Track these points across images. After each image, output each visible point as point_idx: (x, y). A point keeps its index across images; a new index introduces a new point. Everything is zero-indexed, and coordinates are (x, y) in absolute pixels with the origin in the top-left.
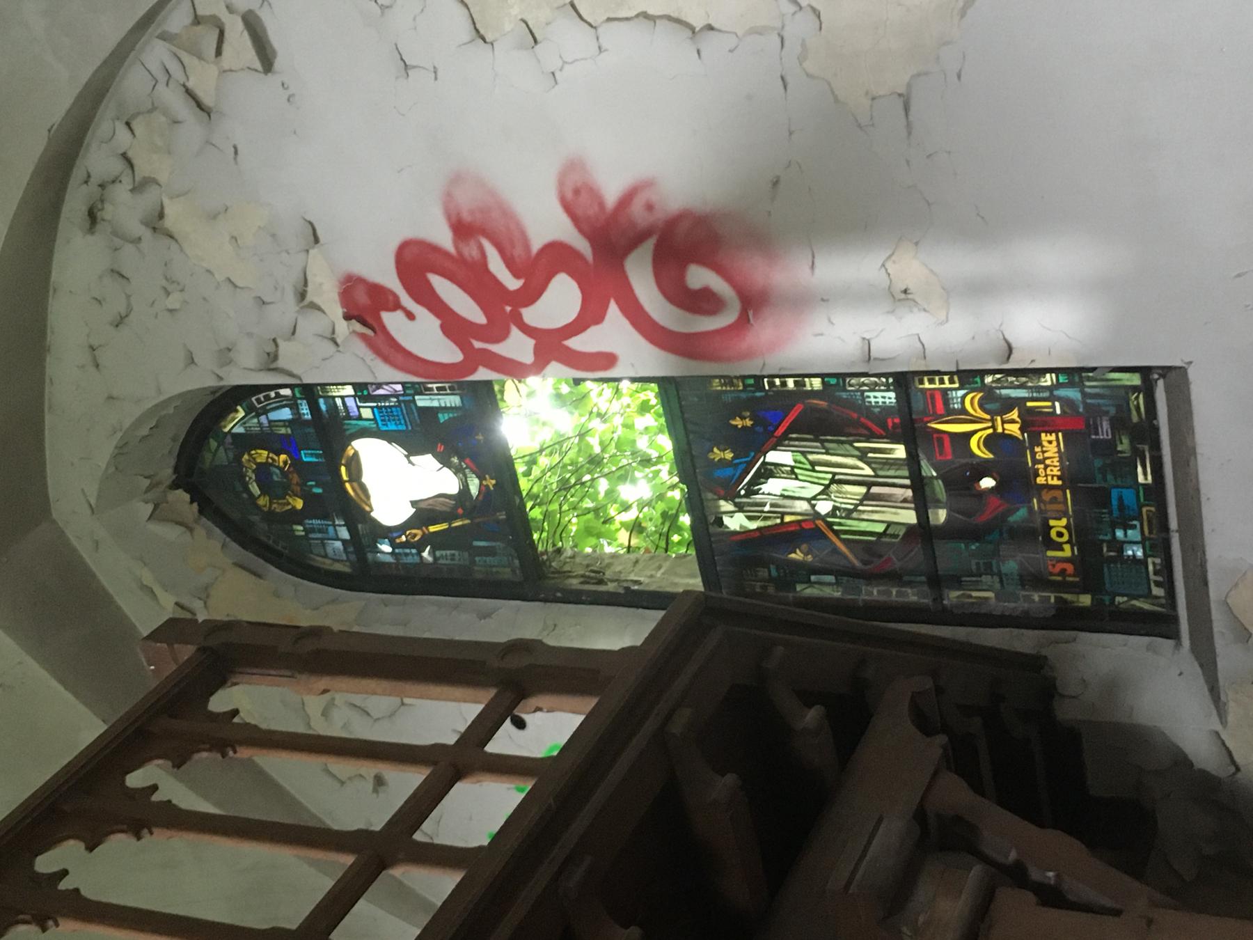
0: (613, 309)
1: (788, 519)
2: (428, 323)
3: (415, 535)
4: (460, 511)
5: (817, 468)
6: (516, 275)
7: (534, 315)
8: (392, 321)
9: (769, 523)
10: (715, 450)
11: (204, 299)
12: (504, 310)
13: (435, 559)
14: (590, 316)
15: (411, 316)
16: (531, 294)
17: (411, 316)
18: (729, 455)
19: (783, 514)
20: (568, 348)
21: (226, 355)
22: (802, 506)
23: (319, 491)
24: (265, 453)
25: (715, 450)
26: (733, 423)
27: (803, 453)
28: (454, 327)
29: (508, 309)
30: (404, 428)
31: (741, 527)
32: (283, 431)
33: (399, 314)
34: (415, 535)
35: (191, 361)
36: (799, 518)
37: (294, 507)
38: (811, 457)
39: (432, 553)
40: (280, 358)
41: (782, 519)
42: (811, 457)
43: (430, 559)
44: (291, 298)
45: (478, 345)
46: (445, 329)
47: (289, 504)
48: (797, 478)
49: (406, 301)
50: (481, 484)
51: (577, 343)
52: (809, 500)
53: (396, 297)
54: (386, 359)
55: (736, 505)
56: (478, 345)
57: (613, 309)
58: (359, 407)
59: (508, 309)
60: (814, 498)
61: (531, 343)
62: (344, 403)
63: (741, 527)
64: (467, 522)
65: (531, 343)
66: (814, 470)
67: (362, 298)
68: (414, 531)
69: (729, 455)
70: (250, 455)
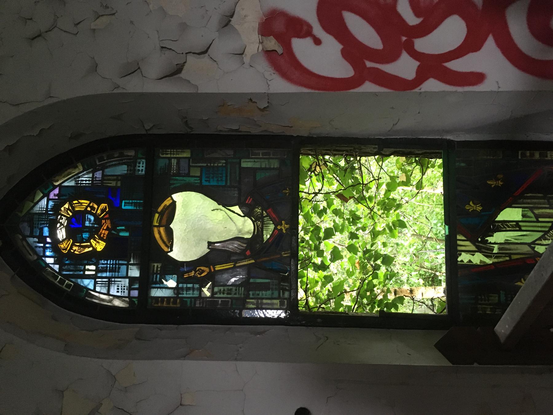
0: (490, 43)
1: (514, 257)
2: (332, 46)
3: (203, 271)
4: (248, 253)
5: (540, 220)
6: (417, 14)
7: (423, 45)
8: (301, 47)
9: (501, 260)
10: (471, 203)
11: (132, 22)
12: (400, 39)
13: (213, 293)
14: (471, 44)
15: (318, 42)
16: (424, 29)
17: (318, 42)
18: (479, 208)
19: (510, 255)
20: (446, 68)
21: (134, 69)
22: (526, 249)
23: (126, 234)
24: (85, 202)
25: (471, 203)
26: (489, 182)
27: (531, 209)
28: (353, 50)
29: (404, 39)
30: (224, 184)
31: (481, 261)
32: (113, 184)
33: (308, 41)
34: (203, 271)
35: (94, 68)
36: (527, 256)
37: (94, 249)
38: (536, 212)
39: (211, 289)
40: (183, 72)
41: (510, 257)
42: (536, 212)
43: (208, 294)
44: (215, 21)
45: (369, 64)
46: (345, 54)
47: (91, 246)
48: (520, 230)
49: (318, 30)
50: (275, 228)
51: (456, 65)
52: (529, 244)
53: (310, 27)
54: (284, 75)
55: (477, 247)
56: (369, 64)
57: (490, 43)
58: (189, 166)
59: (404, 39)
60: (534, 243)
61: (415, 64)
62: (178, 163)
63: (481, 261)
64: (253, 261)
65: (415, 64)
66: (538, 221)
67: (279, 26)
68: (202, 268)
69: (479, 208)
70: (71, 204)
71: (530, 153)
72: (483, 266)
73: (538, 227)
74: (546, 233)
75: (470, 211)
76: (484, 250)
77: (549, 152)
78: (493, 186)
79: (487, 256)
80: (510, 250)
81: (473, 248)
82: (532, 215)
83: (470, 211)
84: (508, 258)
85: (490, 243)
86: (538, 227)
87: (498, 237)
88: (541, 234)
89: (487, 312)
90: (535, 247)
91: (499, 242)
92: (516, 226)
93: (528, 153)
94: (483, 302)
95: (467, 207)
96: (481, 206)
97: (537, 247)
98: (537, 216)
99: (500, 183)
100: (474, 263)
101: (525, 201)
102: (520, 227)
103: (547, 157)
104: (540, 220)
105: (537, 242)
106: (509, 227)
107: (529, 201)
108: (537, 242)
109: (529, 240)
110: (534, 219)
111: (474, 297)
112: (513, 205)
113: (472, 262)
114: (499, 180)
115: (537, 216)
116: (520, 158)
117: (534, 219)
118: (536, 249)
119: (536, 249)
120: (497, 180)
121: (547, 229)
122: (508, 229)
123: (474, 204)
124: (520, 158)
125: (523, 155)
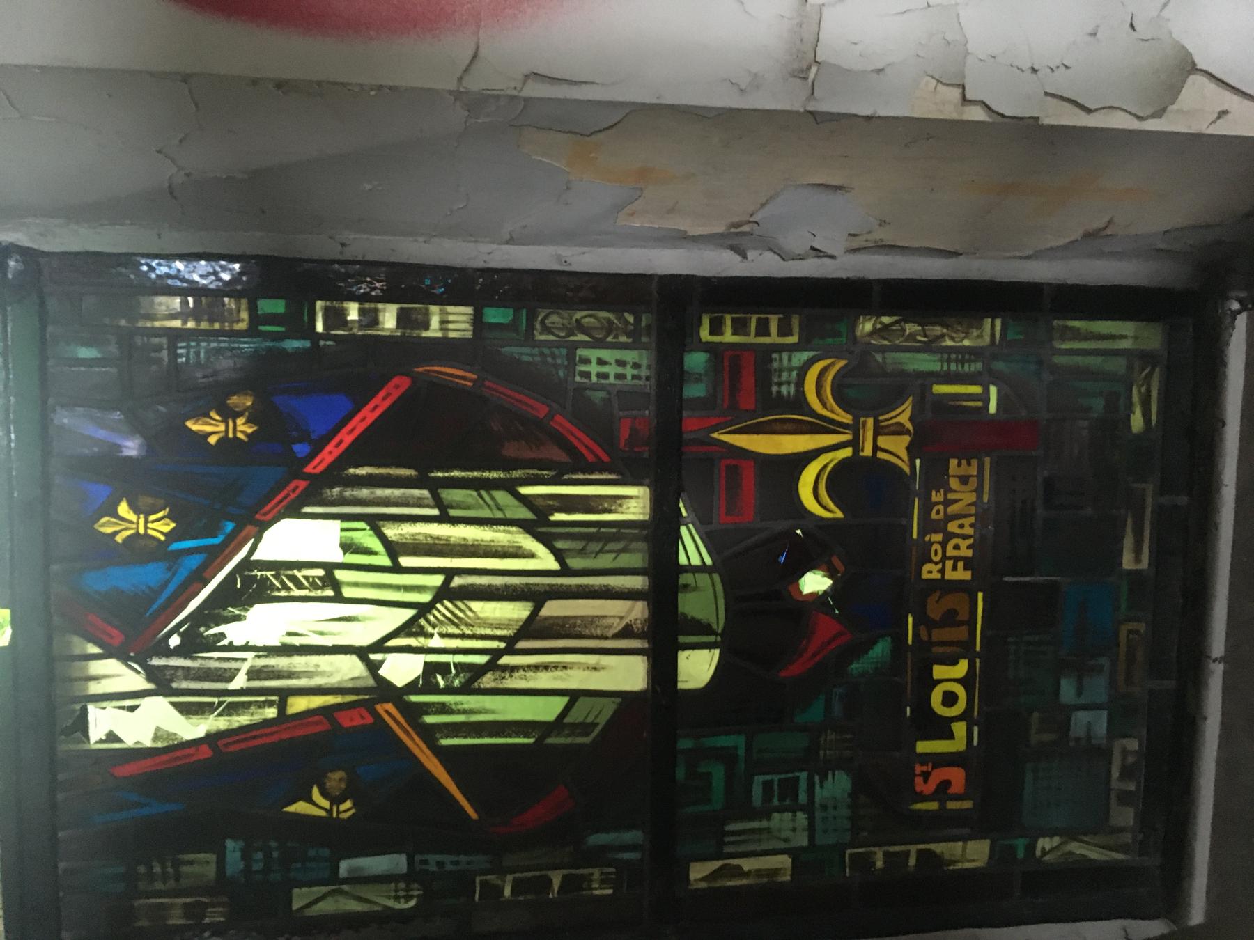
1: (298, 705)
5: (405, 561)
9: (243, 720)
10: (123, 509)
18: (160, 526)
19: (285, 694)
22: (349, 669)
25: (123, 509)
26: (194, 426)
27: (374, 523)
38: (392, 532)
41: (282, 706)
42: (392, 532)
48: (339, 598)
52: (361, 653)
55: (151, 674)
66: (396, 569)
69: (160, 526)
71: (362, 312)
72: (172, 752)
73: (398, 588)
74: (423, 609)
75: (119, 539)
76: (185, 685)
77: (434, 309)
78: (213, 440)
79: (186, 710)
80: (290, 675)
81: (138, 682)
82: (376, 544)
83: (119, 539)
84: (271, 713)
85: (231, 648)
86: (398, 588)
87: (261, 625)
88: (409, 613)
89: (171, 922)
90: (381, 663)
91: (260, 644)
92: (328, 582)
93: (353, 312)
94: (158, 885)
95: (106, 526)
96: (170, 516)
97: (391, 658)
98: (394, 549)
99: (243, 428)
100: (129, 741)
101: (348, 493)
102: (336, 585)
103: (426, 326)
104: (405, 561)
105: (393, 643)
106: (299, 586)
107: (364, 493)
108: (393, 643)
109: (363, 635)
110: (385, 561)
111: (122, 870)
112: (307, 510)
113: (119, 740)
114: (240, 414)
115: (394, 549)
116: (320, 327)
117: (385, 561)
118: (382, 672)
119: (382, 672)
120: (229, 414)
121: (425, 598)
122: (296, 592)
123: (137, 511)
124: (320, 327)
125: (336, 318)
